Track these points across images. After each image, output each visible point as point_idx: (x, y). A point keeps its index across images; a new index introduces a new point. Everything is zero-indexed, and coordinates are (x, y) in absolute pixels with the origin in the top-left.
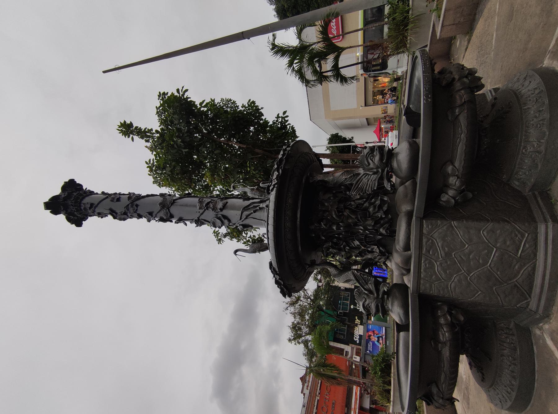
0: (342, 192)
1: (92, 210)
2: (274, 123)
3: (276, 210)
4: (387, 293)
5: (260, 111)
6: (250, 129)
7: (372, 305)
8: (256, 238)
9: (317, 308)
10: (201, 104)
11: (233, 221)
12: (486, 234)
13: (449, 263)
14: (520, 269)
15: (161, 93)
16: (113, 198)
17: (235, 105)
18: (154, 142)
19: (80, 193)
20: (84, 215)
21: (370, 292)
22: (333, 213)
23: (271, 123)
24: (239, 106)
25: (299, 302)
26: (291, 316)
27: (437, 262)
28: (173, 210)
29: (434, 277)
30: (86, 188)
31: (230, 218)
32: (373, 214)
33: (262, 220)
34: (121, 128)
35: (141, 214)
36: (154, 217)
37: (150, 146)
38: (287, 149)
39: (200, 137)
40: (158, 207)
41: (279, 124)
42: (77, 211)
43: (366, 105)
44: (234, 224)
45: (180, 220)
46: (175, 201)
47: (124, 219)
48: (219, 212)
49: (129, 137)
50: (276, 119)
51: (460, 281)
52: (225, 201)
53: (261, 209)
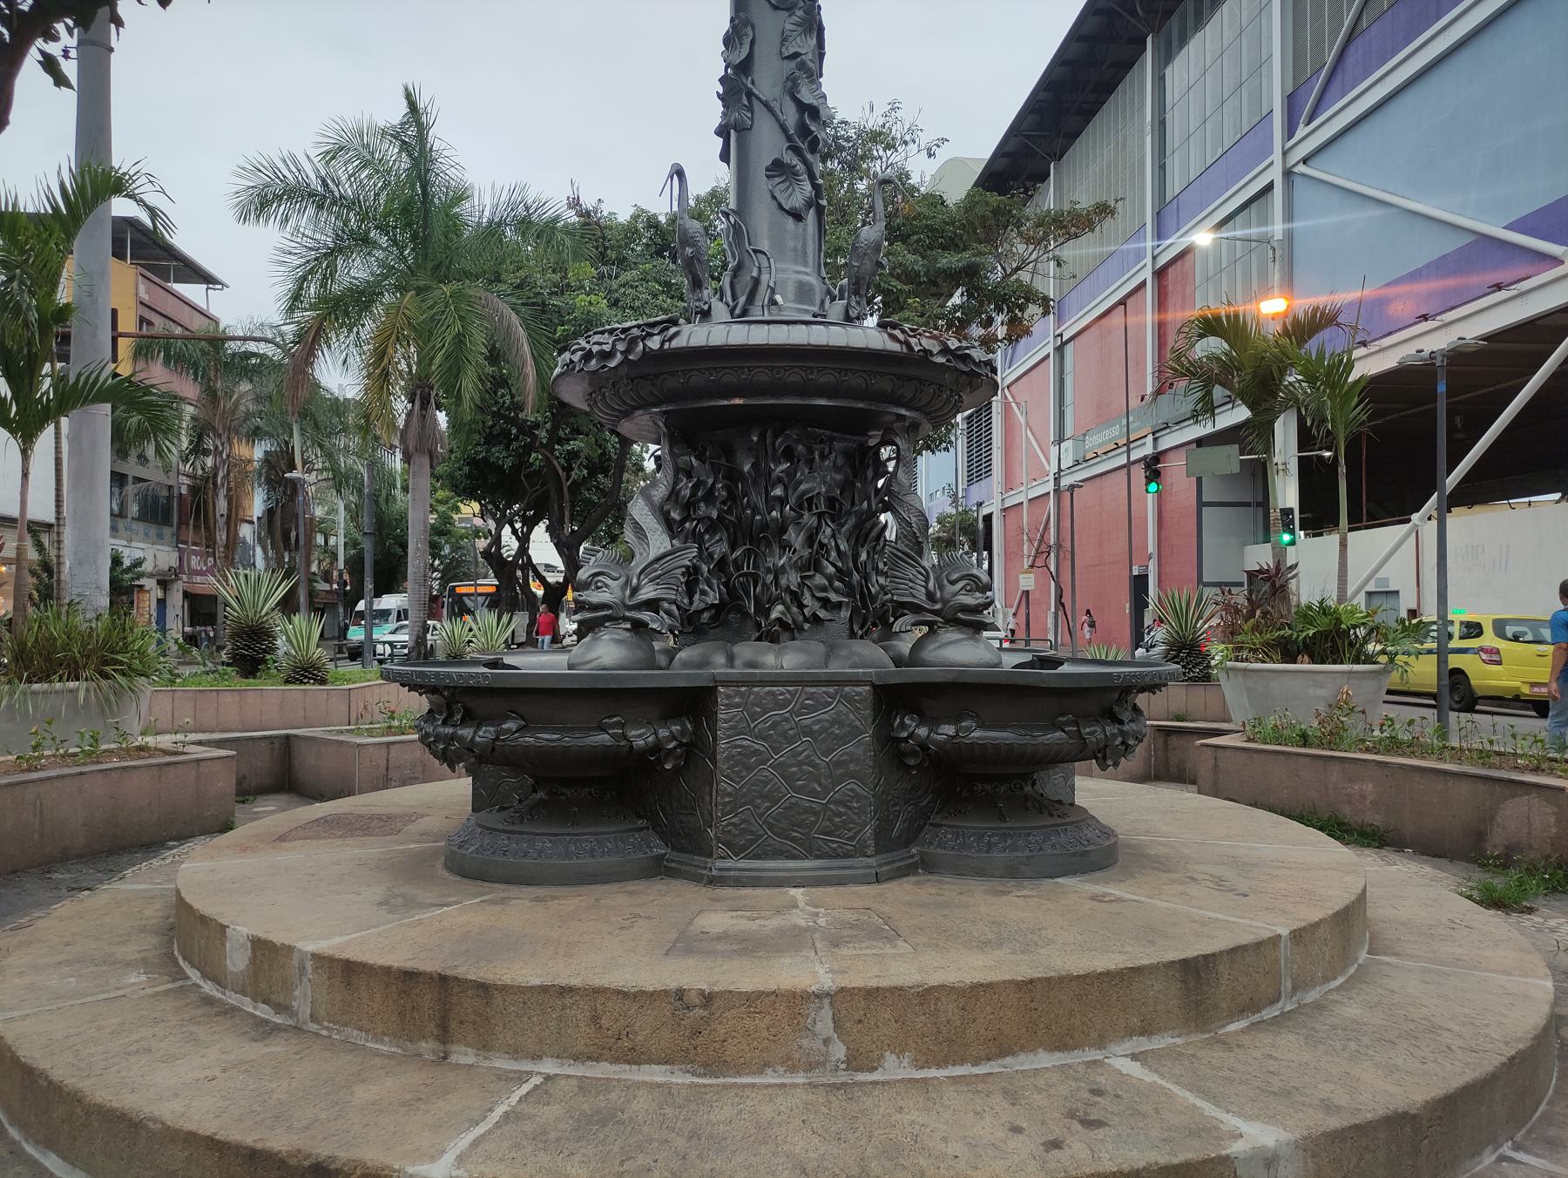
0: (853, 504)
4: (638, 627)
7: (607, 595)
12: (848, 787)
14: (794, 840)
21: (635, 591)
32: (808, 586)
51: (756, 753)
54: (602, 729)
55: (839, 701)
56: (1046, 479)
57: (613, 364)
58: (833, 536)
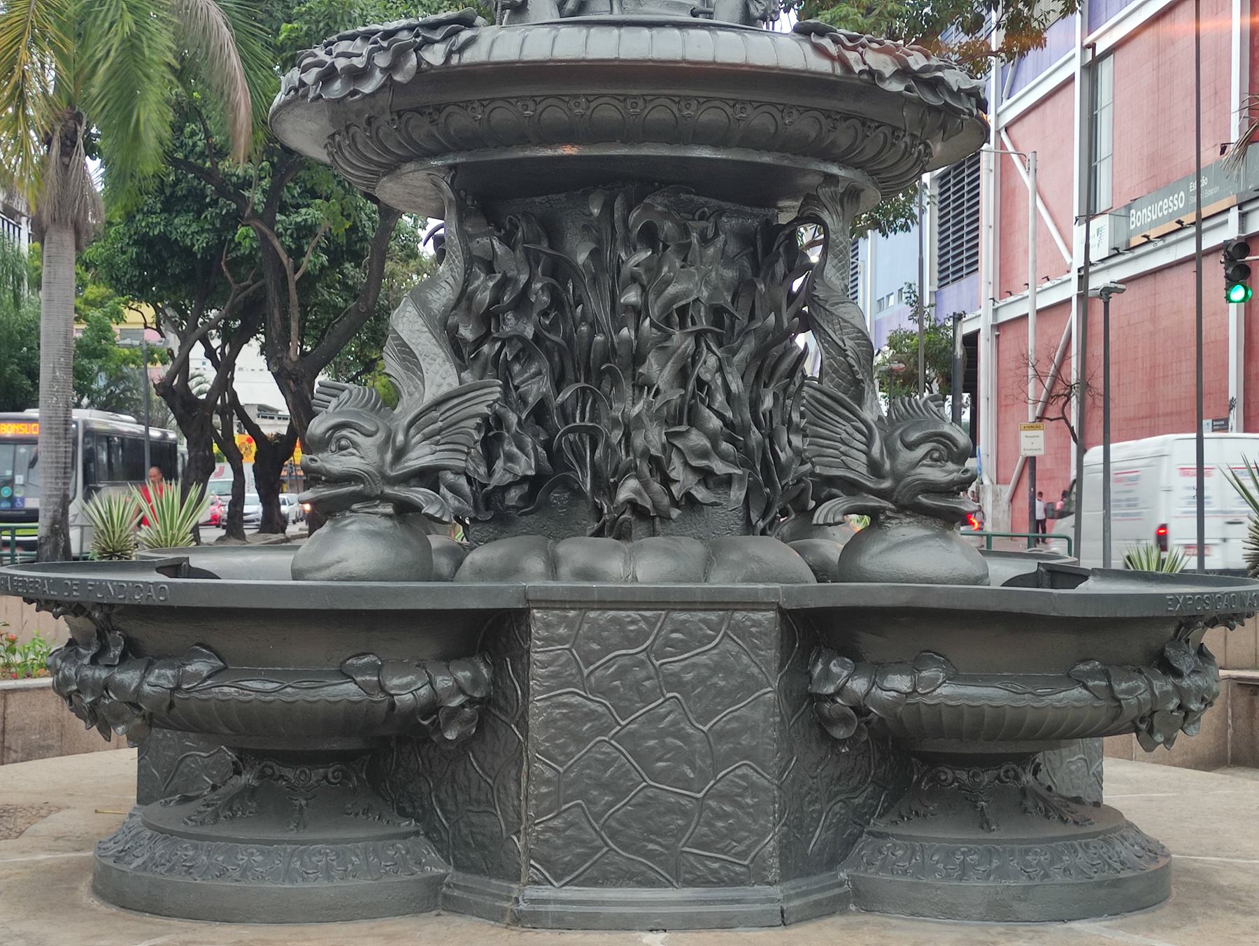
0: (752, 317)
4: (405, 511)
12: (739, 772)
13: (647, 683)
14: (650, 855)
21: (400, 454)
27: (644, 653)
29: (595, 647)
54: (346, 674)
55: (726, 634)
56: (1066, 277)
57: (368, 88)
58: (720, 369)
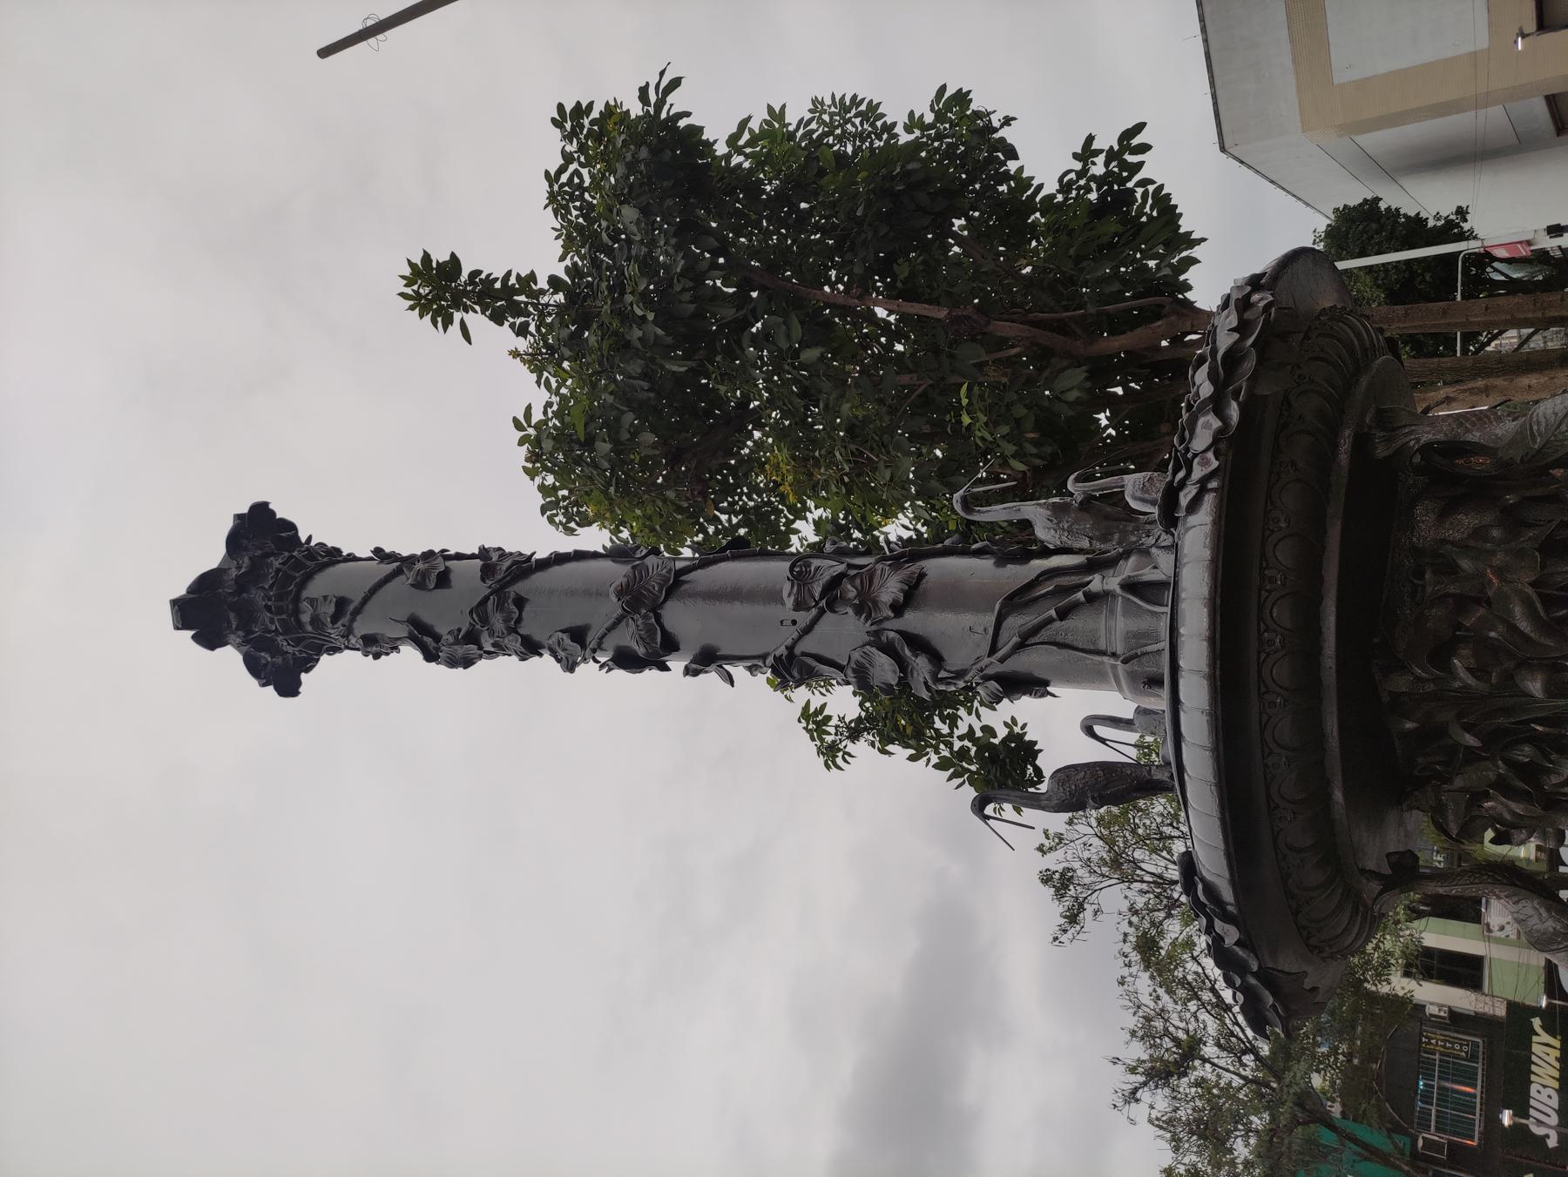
1: (343, 626)
2: (1065, 187)
3: (1218, 601)
5: (997, 136)
6: (953, 228)
8: (996, 741)
9: (1296, 1104)
10: (732, 141)
11: (954, 661)
15: (568, 110)
16: (423, 575)
17: (879, 124)
18: (544, 330)
19: (294, 557)
20: (310, 646)
22: (1518, 611)
23: (1051, 187)
24: (894, 124)
25: (1195, 1069)
26: (1158, 1139)
28: (677, 616)
30: (310, 538)
31: (938, 644)
33: (1103, 653)
34: (415, 287)
35: (538, 637)
36: (594, 651)
37: (530, 350)
38: (1255, 297)
39: (731, 290)
40: (613, 607)
41: (1094, 186)
42: (287, 631)
43: (1543, 25)
44: (960, 674)
45: (706, 659)
46: (683, 578)
47: (467, 662)
48: (887, 618)
49: (448, 322)
50: (1078, 166)
52: (914, 568)
53: (1092, 598)
